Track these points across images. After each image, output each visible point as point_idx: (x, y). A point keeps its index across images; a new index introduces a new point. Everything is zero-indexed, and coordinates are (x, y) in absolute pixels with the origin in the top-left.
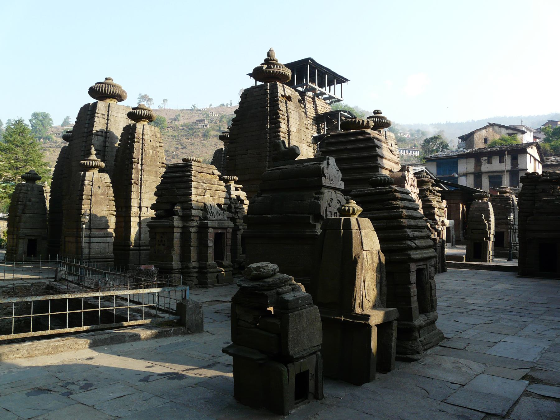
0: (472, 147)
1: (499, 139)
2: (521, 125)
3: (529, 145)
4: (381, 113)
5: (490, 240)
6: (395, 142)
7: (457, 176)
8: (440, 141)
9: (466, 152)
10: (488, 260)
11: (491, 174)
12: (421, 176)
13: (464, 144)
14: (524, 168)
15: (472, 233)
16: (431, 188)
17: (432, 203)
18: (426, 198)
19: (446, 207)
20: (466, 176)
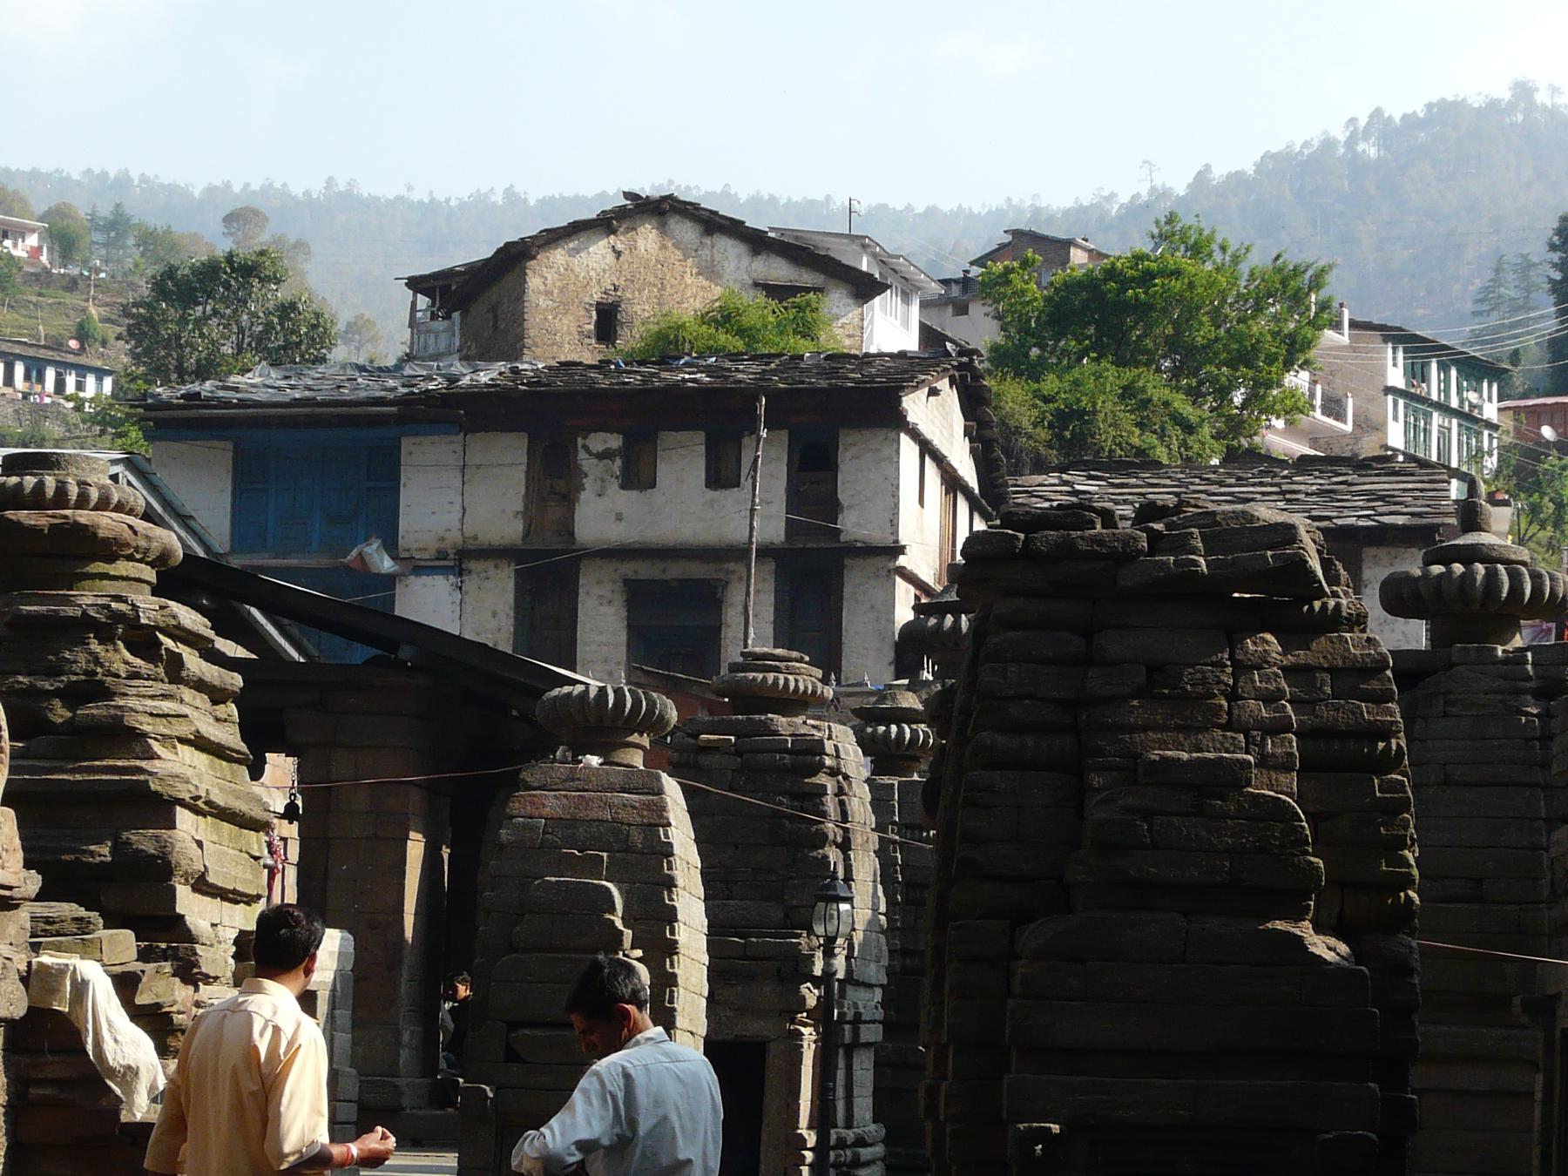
0: (514, 353)
1: (705, 319)
2: (851, 238)
7: (387, 565)
8: (283, 294)
9: (465, 381)
11: (644, 570)
12: (61, 489)
13: (448, 333)
14: (878, 536)
15: (512, 1056)
16: (148, 606)
17: (153, 756)
18: (94, 710)
19: (290, 813)
20: (460, 572)
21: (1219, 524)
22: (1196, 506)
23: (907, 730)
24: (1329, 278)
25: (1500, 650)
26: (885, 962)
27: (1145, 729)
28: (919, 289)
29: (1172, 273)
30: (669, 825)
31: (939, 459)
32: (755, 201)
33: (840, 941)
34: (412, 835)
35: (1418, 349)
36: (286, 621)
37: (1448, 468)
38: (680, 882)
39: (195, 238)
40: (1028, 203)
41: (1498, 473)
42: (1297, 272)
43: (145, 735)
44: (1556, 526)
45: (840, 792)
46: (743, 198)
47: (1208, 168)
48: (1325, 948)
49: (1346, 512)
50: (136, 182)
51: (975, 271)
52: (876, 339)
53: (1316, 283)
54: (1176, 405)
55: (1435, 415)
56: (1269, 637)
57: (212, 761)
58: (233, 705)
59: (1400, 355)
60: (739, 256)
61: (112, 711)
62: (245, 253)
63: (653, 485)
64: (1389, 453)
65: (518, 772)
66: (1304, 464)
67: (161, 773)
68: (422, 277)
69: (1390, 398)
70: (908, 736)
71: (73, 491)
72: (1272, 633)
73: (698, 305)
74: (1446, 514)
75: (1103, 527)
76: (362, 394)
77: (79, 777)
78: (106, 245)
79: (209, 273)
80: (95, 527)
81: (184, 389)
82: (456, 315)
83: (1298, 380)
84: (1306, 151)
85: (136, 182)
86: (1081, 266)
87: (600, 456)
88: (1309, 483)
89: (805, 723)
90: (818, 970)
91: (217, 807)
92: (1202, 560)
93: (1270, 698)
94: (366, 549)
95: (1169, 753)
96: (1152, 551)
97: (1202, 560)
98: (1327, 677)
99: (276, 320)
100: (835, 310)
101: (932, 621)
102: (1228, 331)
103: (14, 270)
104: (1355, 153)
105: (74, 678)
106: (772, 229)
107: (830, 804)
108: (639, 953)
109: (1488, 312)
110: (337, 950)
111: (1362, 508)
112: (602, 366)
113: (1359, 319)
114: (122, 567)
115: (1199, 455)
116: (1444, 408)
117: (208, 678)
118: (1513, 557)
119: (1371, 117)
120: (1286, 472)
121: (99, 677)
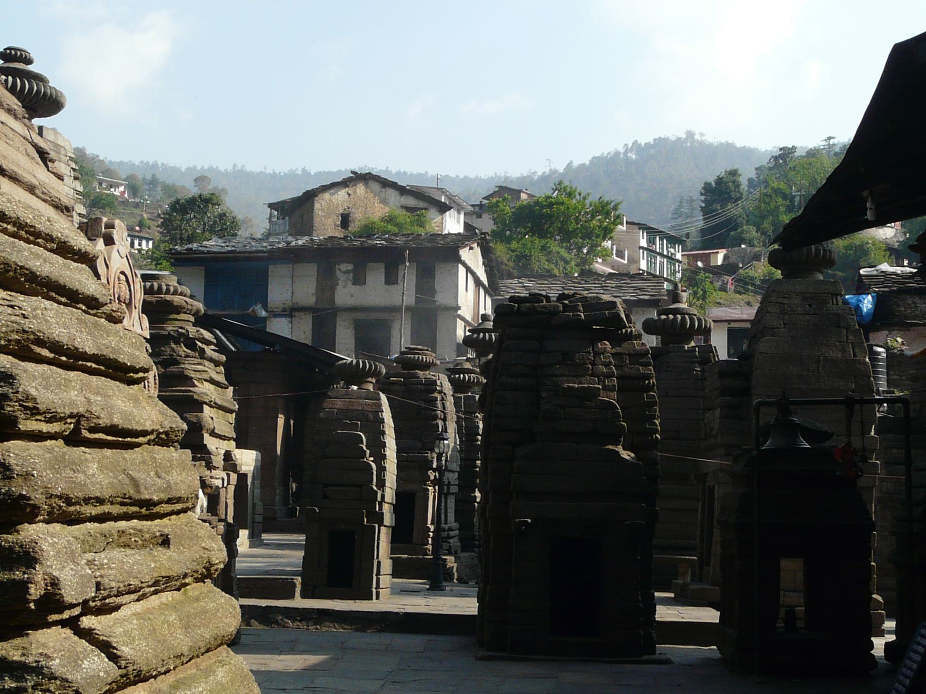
0: (310, 233)
1: (383, 220)
3: (459, 241)
4: (29, 61)
5: (381, 524)
6: (74, 170)
7: (264, 314)
8: (219, 210)
9: (293, 244)
10: (374, 591)
11: (361, 316)
12: (160, 287)
13: (284, 225)
16: (192, 331)
17: (195, 386)
18: (173, 369)
20: (291, 316)
21: (588, 301)
22: (580, 295)
23: (467, 377)
24: (619, 206)
25: (686, 347)
26: (459, 463)
27: (562, 376)
28: (463, 208)
29: (560, 203)
30: (383, 411)
31: (474, 274)
32: (398, 173)
33: (444, 455)
34: (280, 415)
35: (652, 233)
36: (229, 335)
37: (663, 277)
38: (387, 433)
39: (183, 187)
40: (503, 175)
41: (681, 280)
42: (608, 204)
43: (192, 378)
44: (703, 299)
45: (443, 399)
46: (394, 172)
47: (571, 162)
48: (626, 455)
49: (626, 294)
50: (160, 166)
51: (485, 202)
52: (447, 227)
53: (615, 208)
54: (561, 253)
55: (658, 257)
56: (606, 342)
57: (215, 388)
58: (222, 368)
59: (645, 234)
60: (396, 196)
61: (180, 369)
62: (206, 193)
63: (365, 284)
64: (641, 272)
65: (327, 392)
66: (611, 276)
67: (198, 392)
68: (274, 203)
69: (641, 251)
70: (467, 379)
71: (164, 288)
72: (608, 341)
73: (380, 214)
74: (664, 295)
75: (546, 302)
76: (254, 249)
77: (168, 394)
78: (149, 190)
79: (192, 202)
80: (173, 301)
81: (186, 247)
82: (287, 218)
83: (607, 244)
84: (609, 156)
85: (160, 166)
86: (526, 200)
87: (345, 272)
88: (612, 283)
89: (429, 374)
90: (435, 466)
91: (218, 405)
92: (582, 314)
93: (607, 365)
94: (256, 308)
95: (571, 385)
96: (564, 311)
97: (582, 314)
98: (627, 357)
99: (218, 220)
100: (432, 217)
101: (475, 336)
102: (581, 225)
103: (115, 200)
104: (627, 157)
105: (165, 357)
106: (408, 186)
107: (439, 404)
108: (372, 459)
109: (677, 218)
110: (254, 458)
111: (632, 293)
112: (345, 238)
113: (629, 220)
114: (183, 316)
115: (570, 272)
116: (659, 254)
117: (214, 357)
118: (691, 313)
119: (633, 143)
120: (603, 279)
121: (175, 357)
